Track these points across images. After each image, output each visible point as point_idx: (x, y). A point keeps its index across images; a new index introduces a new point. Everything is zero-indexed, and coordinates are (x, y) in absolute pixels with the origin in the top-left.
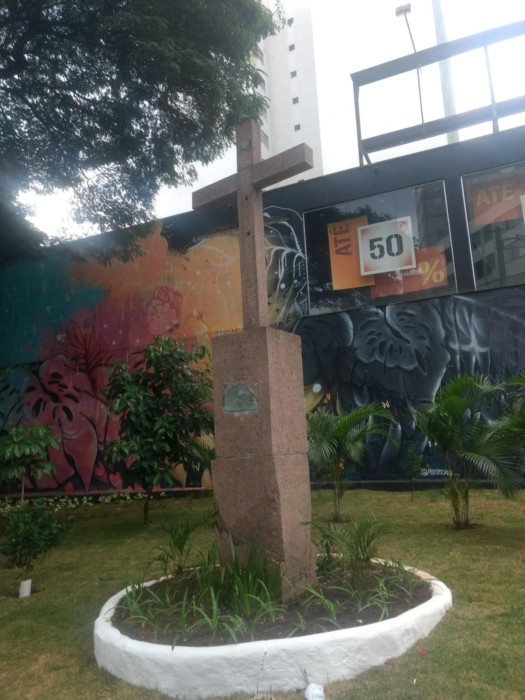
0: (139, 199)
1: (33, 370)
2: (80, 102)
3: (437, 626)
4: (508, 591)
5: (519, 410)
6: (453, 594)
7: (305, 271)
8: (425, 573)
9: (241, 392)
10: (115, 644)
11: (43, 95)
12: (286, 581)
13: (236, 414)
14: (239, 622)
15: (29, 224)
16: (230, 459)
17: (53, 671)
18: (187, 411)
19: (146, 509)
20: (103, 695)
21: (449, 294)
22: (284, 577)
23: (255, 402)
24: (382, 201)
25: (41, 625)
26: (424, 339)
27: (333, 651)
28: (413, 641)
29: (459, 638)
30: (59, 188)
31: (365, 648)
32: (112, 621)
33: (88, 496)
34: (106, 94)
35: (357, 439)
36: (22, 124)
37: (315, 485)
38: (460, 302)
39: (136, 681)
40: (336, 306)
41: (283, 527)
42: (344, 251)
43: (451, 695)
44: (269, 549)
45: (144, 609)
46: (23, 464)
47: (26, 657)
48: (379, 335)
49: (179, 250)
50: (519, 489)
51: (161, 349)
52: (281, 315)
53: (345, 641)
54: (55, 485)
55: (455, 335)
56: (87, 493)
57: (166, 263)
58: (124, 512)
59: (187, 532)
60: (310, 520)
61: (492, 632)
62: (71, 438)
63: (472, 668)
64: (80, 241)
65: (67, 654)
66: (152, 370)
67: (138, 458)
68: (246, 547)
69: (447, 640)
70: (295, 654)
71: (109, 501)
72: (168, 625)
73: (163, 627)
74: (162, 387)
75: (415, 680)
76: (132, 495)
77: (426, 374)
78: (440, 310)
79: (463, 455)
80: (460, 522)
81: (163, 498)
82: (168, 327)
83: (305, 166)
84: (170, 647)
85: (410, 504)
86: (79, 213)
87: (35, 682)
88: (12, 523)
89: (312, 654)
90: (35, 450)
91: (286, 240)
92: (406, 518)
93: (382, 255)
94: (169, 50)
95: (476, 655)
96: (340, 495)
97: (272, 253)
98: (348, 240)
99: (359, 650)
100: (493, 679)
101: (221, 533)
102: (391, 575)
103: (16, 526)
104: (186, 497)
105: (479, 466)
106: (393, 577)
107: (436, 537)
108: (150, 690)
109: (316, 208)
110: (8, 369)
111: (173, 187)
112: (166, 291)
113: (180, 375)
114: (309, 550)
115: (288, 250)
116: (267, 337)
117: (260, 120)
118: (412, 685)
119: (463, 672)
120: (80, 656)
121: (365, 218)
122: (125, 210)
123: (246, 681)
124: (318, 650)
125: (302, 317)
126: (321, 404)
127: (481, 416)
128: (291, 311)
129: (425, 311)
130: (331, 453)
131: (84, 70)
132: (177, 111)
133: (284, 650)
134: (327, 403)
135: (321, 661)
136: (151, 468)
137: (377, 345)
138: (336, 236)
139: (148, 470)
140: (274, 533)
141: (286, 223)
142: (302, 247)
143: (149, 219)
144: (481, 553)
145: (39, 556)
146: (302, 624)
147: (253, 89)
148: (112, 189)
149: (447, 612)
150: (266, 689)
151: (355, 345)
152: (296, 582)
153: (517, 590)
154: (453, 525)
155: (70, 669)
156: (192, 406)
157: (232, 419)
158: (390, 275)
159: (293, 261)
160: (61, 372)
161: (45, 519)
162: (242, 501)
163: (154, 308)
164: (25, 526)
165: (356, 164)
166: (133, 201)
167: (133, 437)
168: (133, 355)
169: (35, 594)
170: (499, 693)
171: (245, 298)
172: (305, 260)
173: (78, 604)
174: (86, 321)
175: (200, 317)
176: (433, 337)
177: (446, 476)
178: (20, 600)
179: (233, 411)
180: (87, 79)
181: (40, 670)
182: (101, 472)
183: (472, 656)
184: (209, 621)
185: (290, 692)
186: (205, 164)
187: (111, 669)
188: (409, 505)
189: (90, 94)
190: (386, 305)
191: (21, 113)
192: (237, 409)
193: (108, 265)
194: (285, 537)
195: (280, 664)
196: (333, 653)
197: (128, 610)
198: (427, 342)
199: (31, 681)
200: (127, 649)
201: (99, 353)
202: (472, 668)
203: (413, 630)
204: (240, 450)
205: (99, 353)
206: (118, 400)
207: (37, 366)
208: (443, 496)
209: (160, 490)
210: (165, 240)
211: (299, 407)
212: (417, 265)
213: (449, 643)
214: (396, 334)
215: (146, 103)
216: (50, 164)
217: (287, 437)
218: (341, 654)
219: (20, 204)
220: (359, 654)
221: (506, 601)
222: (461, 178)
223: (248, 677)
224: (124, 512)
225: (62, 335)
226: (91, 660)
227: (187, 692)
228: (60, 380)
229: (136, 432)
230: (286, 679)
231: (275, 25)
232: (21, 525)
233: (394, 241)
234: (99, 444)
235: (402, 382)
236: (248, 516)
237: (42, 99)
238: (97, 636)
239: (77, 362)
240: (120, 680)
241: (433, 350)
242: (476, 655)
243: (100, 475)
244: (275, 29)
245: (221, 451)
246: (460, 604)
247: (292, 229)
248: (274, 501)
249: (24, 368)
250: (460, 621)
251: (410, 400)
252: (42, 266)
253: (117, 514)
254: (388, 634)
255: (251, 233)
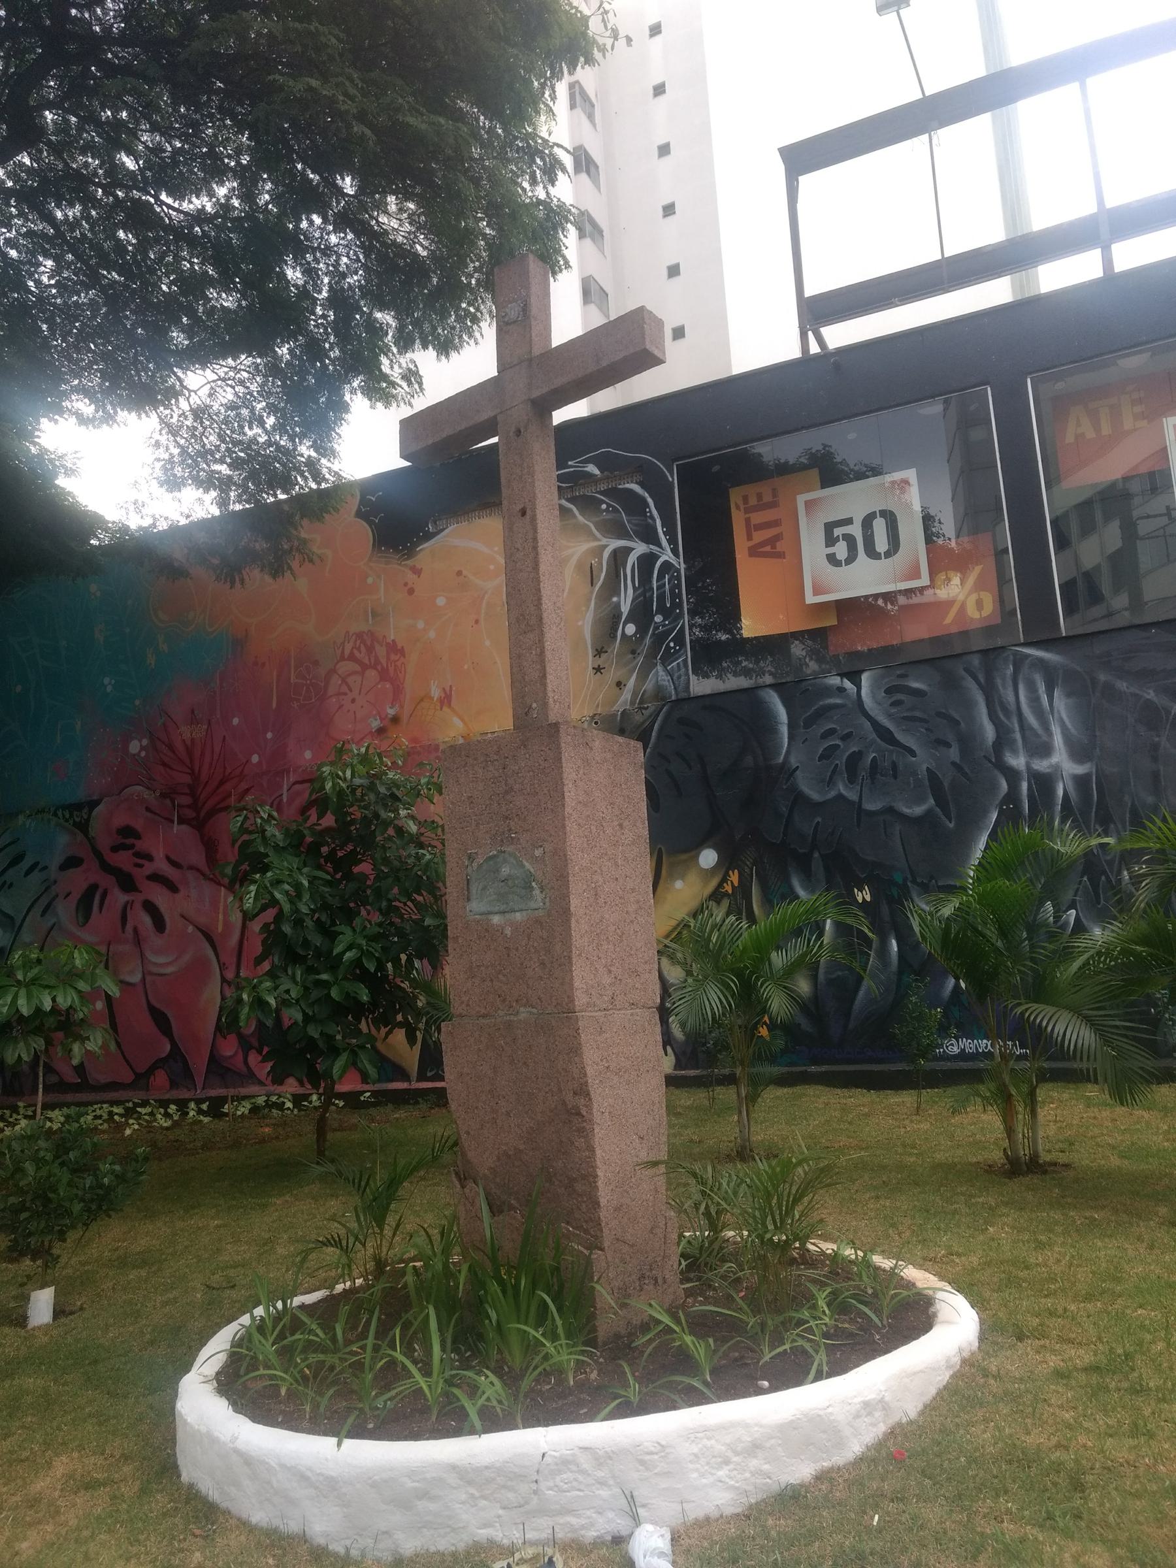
0: (303, 436)
1: (78, 820)
2: (170, 218)
3: (940, 1393)
4: (1108, 1313)
5: (1142, 905)
6: (982, 1322)
7: (680, 595)
8: (928, 1275)
9: (505, 871)
10: (216, 1434)
11: (89, 201)
12: (604, 1295)
13: (496, 919)
14: (491, 1386)
15: (64, 493)
16: (482, 1021)
17: (83, 1492)
18: (409, 910)
19: (321, 1128)
20: (185, 1545)
21: (1003, 645)
22: (598, 1287)
23: (537, 892)
24: (852, 436)
25: (66, 1388)
26: (948, 745)
27: (696, 1450)
28: (882, 1428)
29: (986, 1420)
30: (130, 410)
31: (768, 1445)
32: (218, 1382)
33: (199, 1102)
34: (228, 198)
35: (790, 971)
36: (42, 269)
37: (703, 1076)
38: (1028, 661)
39: (259, 1516)
40: (762, 673)
41: (600, 1173)
42: (768, 548)
43: (954, 1553)
44: (568, 1223)
45: (286, 1353)
46: (38, 1031)
47: (27, 1459)
48: (846, 737)
49: (396, 551)
50: (1149, 1083)
51: (348, 774)
52: (627, 695)
53: (733, 1425)
54: (127, 1076)
55: (1018, 736)
56: (199, 1093)
57: (370, 580)
58: (277, 1138)
59: (393, 1184)
60: (664, 1156)
61: (1061, 1407)
62: (162, 971)
63: (1006, 1492)
64: (174, 530)
65: (117, 1454)
66: (329, 820)
67: (299, 1017)
68: (519, 1217)
69: (957, 1425)
70: (610, 1458)
71: (247, 1112)
72: (331, 1392)
73: (322, 1394)
74: (353, 858)
75: (877, 1517)
76: (298, 1100)
77: (951, 825)
78: (982, 680)
79: (1019, 1010)
80: (1018, 1159)
81: (366, 1105)
82: (375, 724)
83: (645, 360)
84: (334, 1440)
85: (914, 1117)
86: (172, 469)
87: (40, 1515)
88: (8, 1161)
89: (647, 1457)
90: (65, 1001)
91: (636, 525)
92: (900, 1150)
93: (851, 559)
94: (346, 95)
95: (1019, 1461)
96: (752, 1099)
97: (606, 554)
98: (776, 523)
99: (755, 1448)
100: (1050, 1517)
101: (463, 1187)
102: (849, 1279)
103: (19, 1170)
104: (417, 1103)
105: (1055, 1036)
106: (852, 1283)
107: (963, 1194)
108: (288, 1536)
109: (690, 457)
110: (21, 818)
111: (379, 405)
112: (369, 643)
113: (391, 831)
114: (662, 1225)
115: (640, 548)
116: (563, 745)
117: (564, 257)
118: (868, 1529)
119: (984, 1500)
120: (144, 1459)
121: (814, 474)
122: (275, 459)
123: (499, 1517)
124: (663, 1448)
125: (673, 698)
126: (716, 896)
127: (1077, 919)
128: (649, 685)
129: (950, 683)
130: (724, 1007)
131: (179, 145)
132: (382, 234)
133: (585, 1449)
134: (730, 892)
135: (667, 1474)
136: (330, 1038)
137: (841, 760)
138: (750, 515)
139: (321, 1044)
140: (579, 1187)
141: (636, 488)
142: (672, 541)
143: (327, 481)
144: (1059, 1229)
145: (72, 1236)
146: (634, 1390)
147: (545, 187)
148: (245, 412)
149: (964, 1362)
150: (545, 1534)
151: (793, 762)
152: (629, 1295)
153: (1128, 1311)
154: (1003, 1165)
155: (119, 1488)
156: (420, 899)
157: (487, 931)
158: (880, 602)
159: (652, 573)
160: (138, 825)
161: (85, 1154)
162: (508, 1114)
163: (344, 681)
164: (38, 1169)
165: (795, 353)
166: (292, 439)
167: (286, 971)
168: (297, 787)
169: (63, 1320)
170: (1061, 1549)
171: (516, 660)
172: (678, 571)
173: (152, 1342)
174: (193, 712)
175: (446, 699)
176: (968, 741)
177: (989, 1055)
178: (27, 1332)
179: (490, 913)
180: (185, 164)
181: (55, 1489)
182: (229, 1048)
183: (1010, 1462)
184: (423, 1383)
185: (597, 1544)
186: (443, 357)
187: (208, 1488)
188: (912, 1121)
189: (194, 199)
190: (863, 671)
191: (38, 244)
192: (496, 909)
193: (238, 584)
194: (605, 1196)
195: (575, 1480)
196: (696, 1455)
197: (254, 1358)
198: (954, 753)
199: (32, 1512)
200: (240, 1445)
201: (222, 783)
202: (1006, 1492)
203: (882, 1405)
204: (504, 1000)
205: (222, 783)
206: (253, 888)
207: (86, 810)
208: (979, 1100)
209: (359, 1087)
210: (368, 528)
211: (638, 902)
212: (932, 579)
213: (962, 1432)
214: (886, 735)
215: (317, 220)
216: (105, 357)
217: (610, 972)
218: (714, 1457)
219: (44, 451)
220: (755, 1457)
221: (1100, 1339)
222: (1029, 381)
223: (504, 1508)
224: (277, 1138)
225: (140, 741)
226: (168, 1468)
227: (370, 1542)
228: (136, 842)
229: (293, 957)
230: (588, 1513)
231: (595, 42)
232: (29, 1167)
233: (879, 526)
234: (226, 986)
235: (899, 841)
236: (522, 1147)
237: (85, 209)
238: (180, 1413)
239: (173, 803)
240: (226, 1513)
241: (967, 770)
242: (1019, 1461)
243: (229, 1053)
244: (595, 51)
245: (462, 1002)
246: (997, 1343)
247: (650, 500)
248: (579, 1114)
249: (55, 814)
250: (992, 1382)
251: (918, 885)
252: (93, 588)
253: (263, 1141)
254: (821, 1413)
255: (529, 512)
